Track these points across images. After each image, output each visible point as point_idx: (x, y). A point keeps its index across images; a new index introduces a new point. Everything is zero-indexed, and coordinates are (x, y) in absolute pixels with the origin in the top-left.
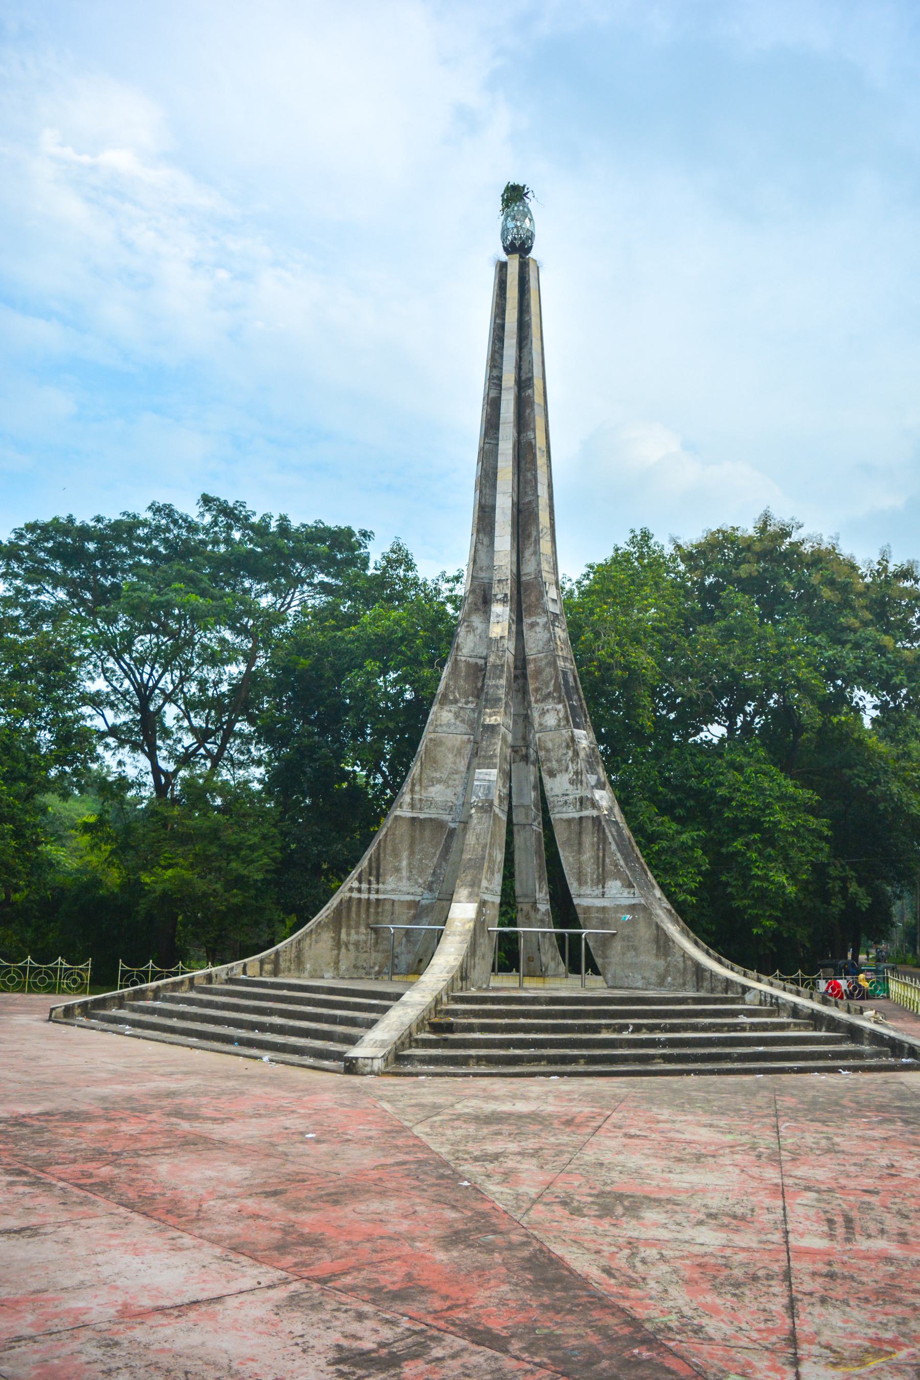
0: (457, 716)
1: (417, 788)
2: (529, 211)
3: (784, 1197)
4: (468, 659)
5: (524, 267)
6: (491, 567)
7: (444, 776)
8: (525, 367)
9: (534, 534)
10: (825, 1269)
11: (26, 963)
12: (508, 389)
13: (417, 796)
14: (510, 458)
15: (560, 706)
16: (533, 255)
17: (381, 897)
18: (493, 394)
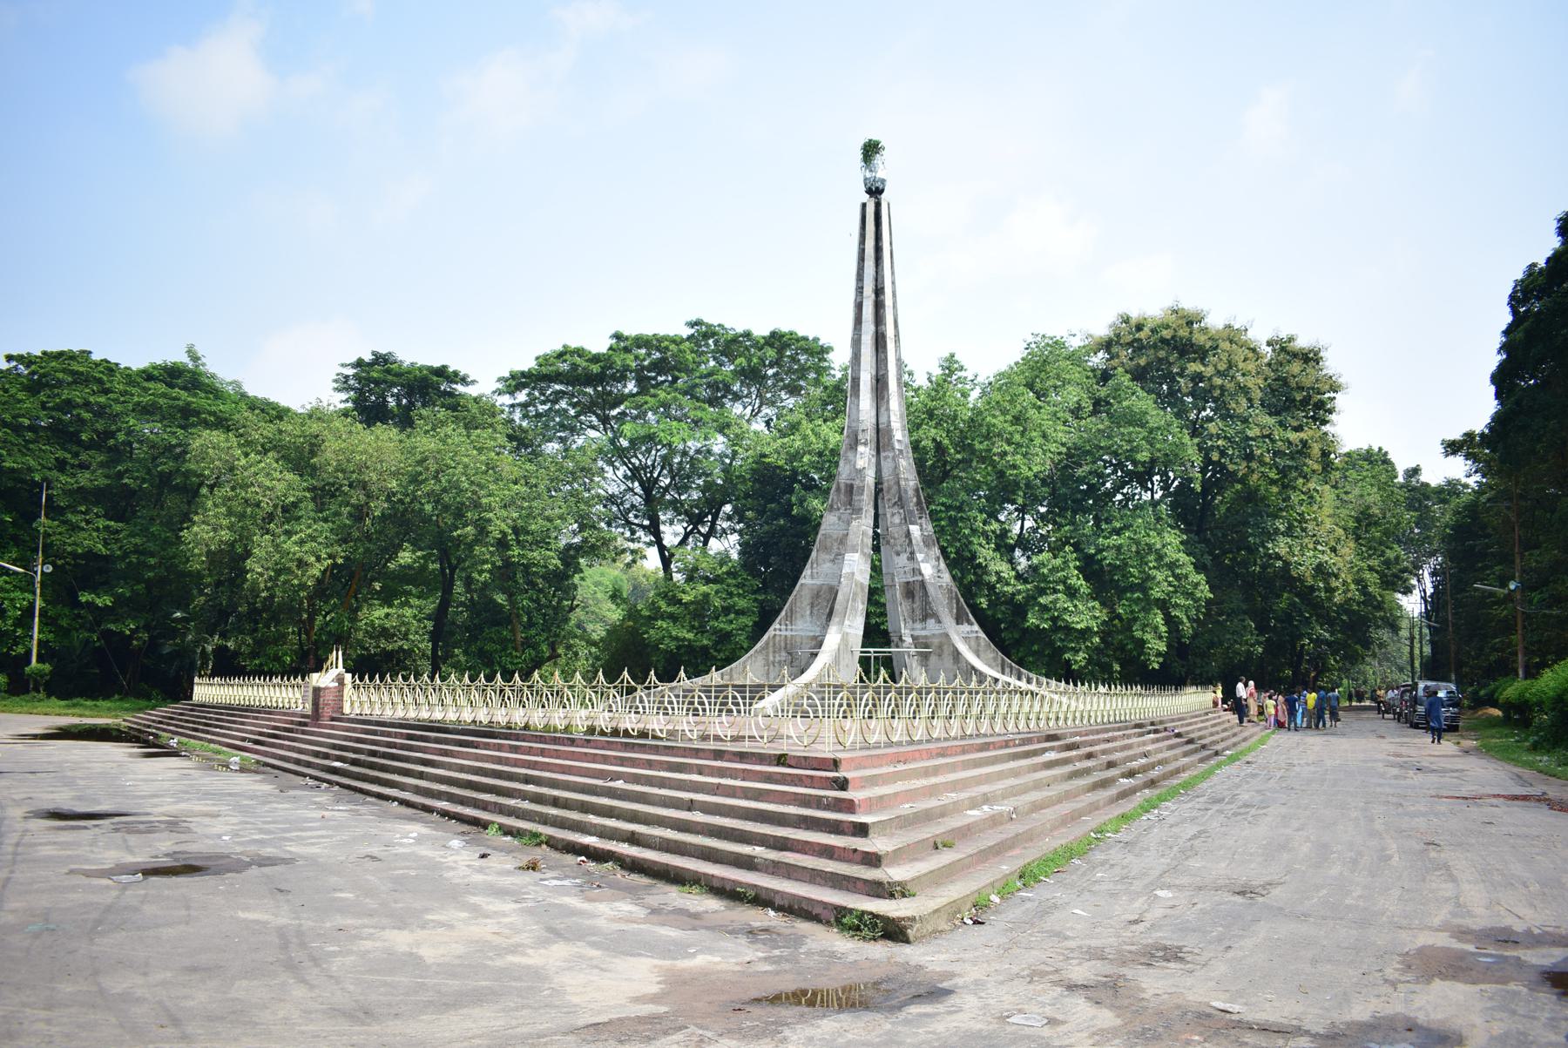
0: (839, 519)
1: (815, 566)
5: (878, 205)
10: (1046, 1021)
11: (622, 682)
13: (815, 571)
14: (869, 346)
15: (902, 511)
16: (883, 196)
17: (793, 633)
18: (858, 300)
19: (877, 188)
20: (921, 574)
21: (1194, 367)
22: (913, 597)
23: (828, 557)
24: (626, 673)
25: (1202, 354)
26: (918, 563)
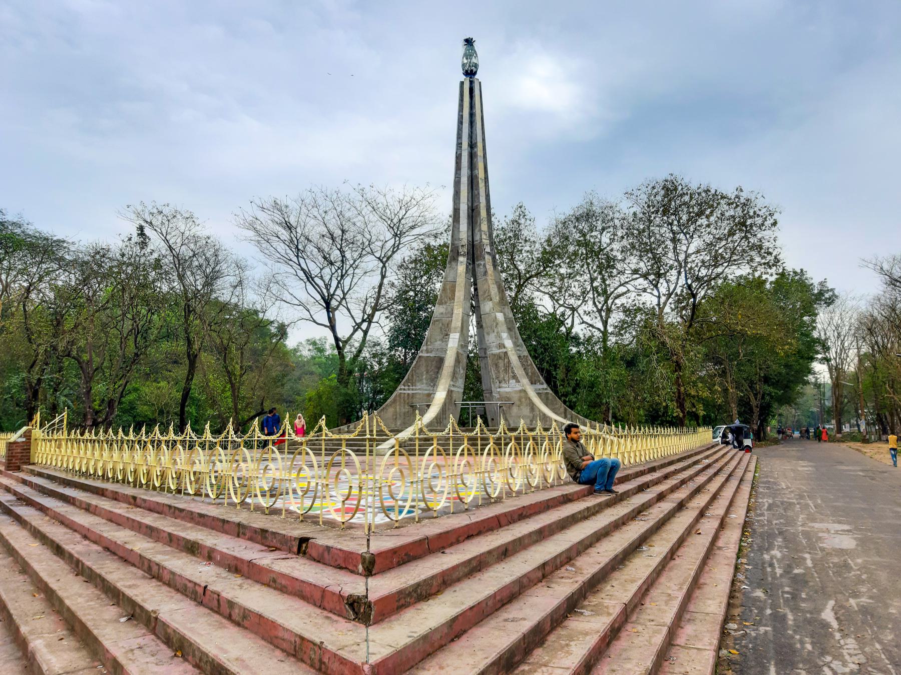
2: (475, 52)
3: (170, 247)
5: (471, 82)
8: (474, 137)
12: (465, 150)
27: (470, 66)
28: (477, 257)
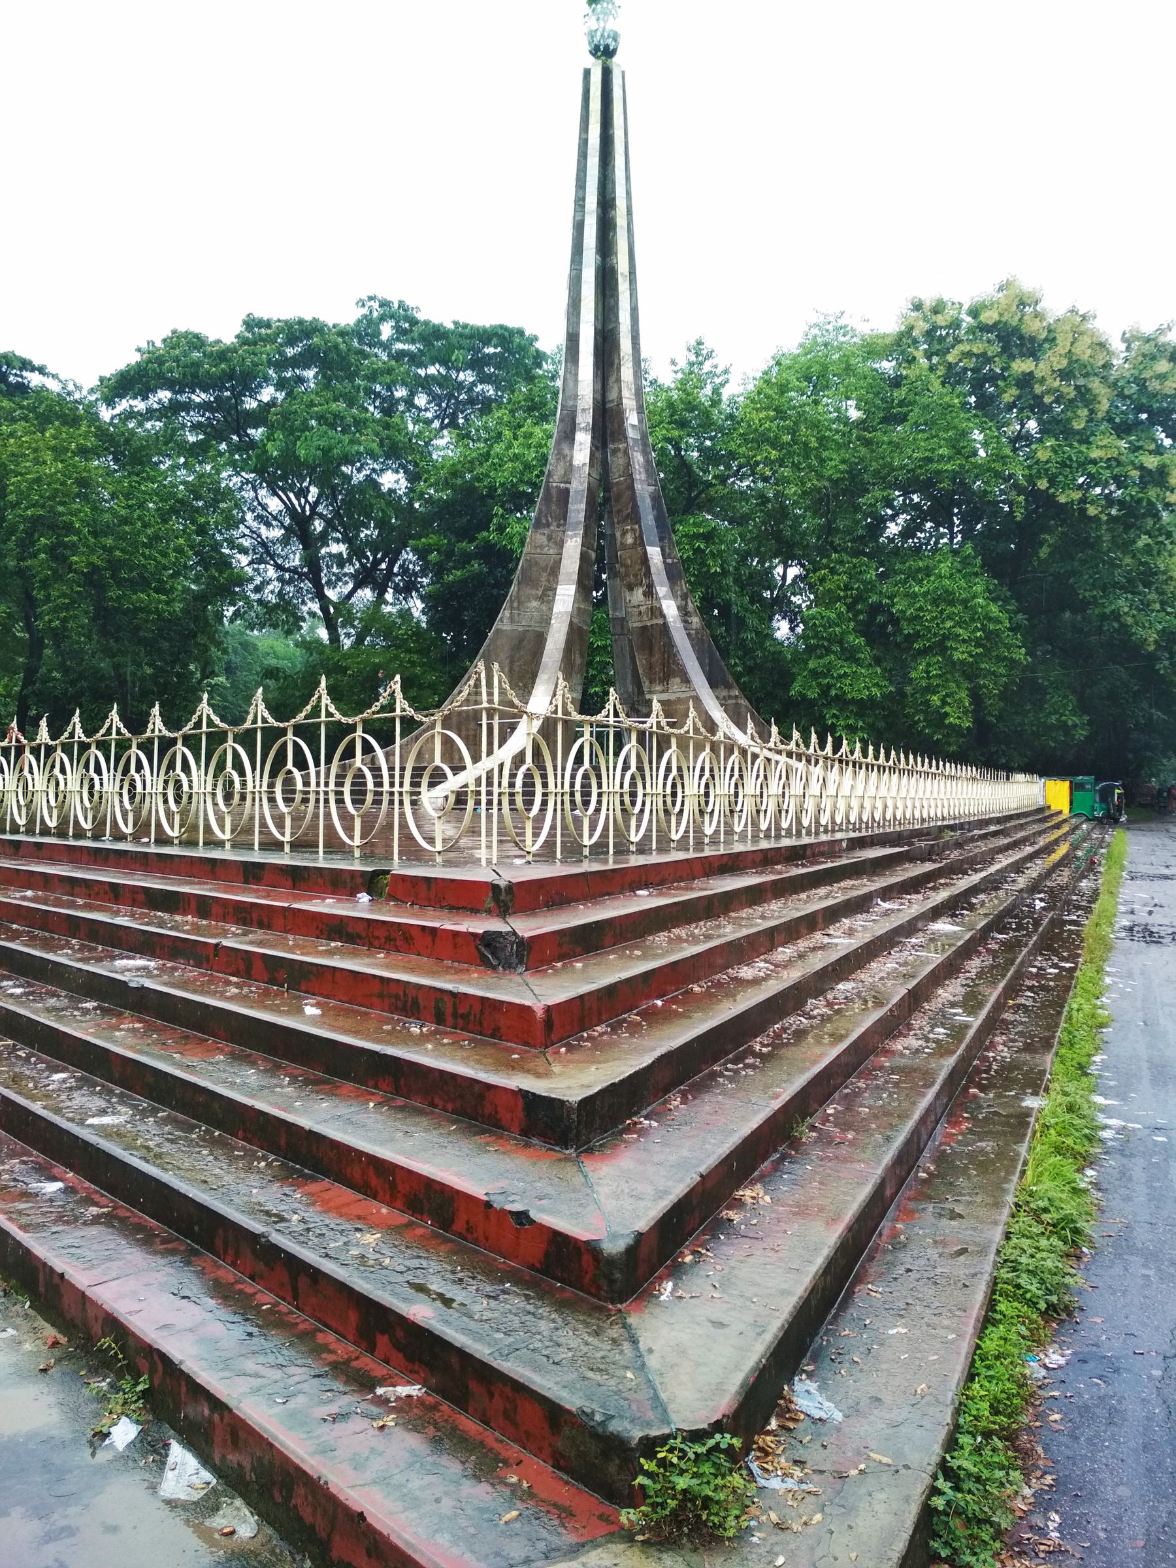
1: (516, 604)
4: (826, 940)
5: (607, 73)
6: (576, 397)
7: (540, 593)
9: (616, 361)
11: (198, 725)
16: (616, 59)
19: (607, 47)
20: (663, 616)
21: (1021, 366)
22: (651, 648)
23: (533, 592)
24: (114, 715)
25: (1032, 348)
26: (658, 599)
27: (602, 35)
28: (613, 433)
